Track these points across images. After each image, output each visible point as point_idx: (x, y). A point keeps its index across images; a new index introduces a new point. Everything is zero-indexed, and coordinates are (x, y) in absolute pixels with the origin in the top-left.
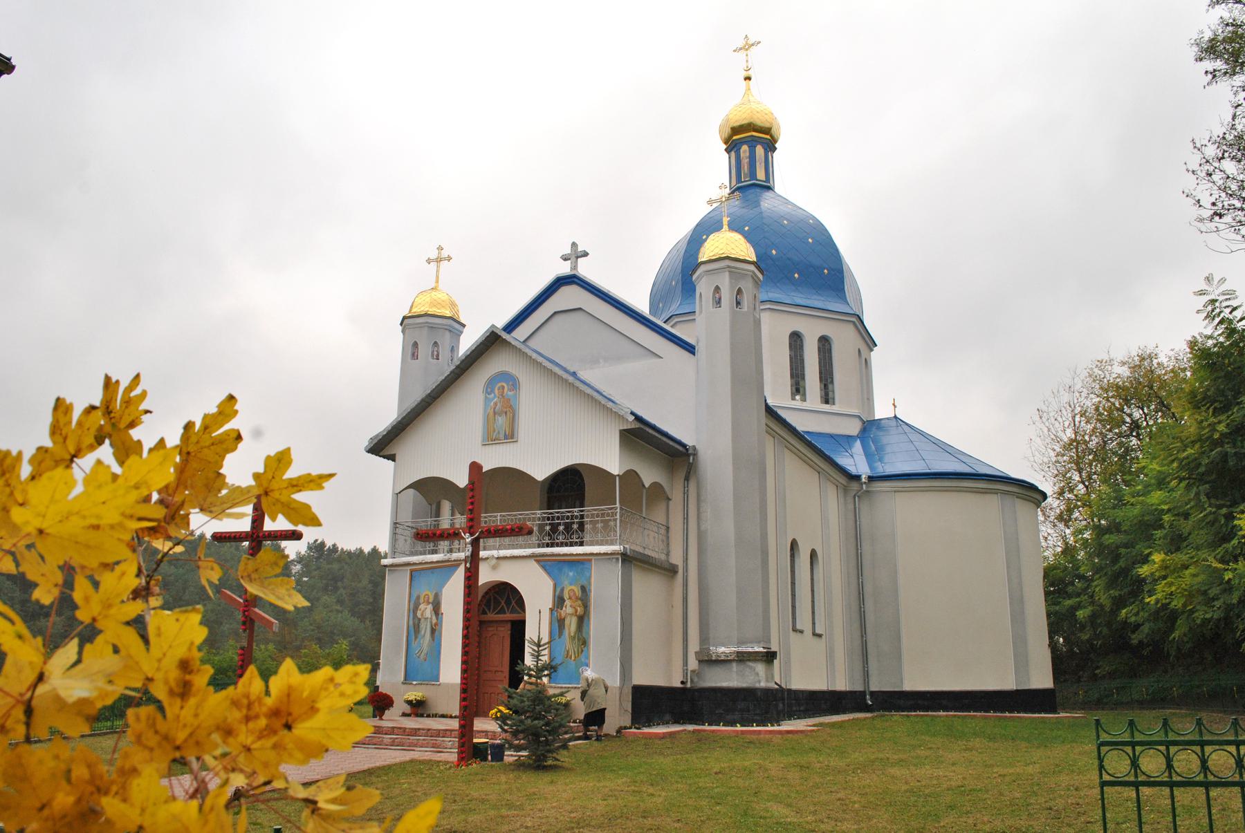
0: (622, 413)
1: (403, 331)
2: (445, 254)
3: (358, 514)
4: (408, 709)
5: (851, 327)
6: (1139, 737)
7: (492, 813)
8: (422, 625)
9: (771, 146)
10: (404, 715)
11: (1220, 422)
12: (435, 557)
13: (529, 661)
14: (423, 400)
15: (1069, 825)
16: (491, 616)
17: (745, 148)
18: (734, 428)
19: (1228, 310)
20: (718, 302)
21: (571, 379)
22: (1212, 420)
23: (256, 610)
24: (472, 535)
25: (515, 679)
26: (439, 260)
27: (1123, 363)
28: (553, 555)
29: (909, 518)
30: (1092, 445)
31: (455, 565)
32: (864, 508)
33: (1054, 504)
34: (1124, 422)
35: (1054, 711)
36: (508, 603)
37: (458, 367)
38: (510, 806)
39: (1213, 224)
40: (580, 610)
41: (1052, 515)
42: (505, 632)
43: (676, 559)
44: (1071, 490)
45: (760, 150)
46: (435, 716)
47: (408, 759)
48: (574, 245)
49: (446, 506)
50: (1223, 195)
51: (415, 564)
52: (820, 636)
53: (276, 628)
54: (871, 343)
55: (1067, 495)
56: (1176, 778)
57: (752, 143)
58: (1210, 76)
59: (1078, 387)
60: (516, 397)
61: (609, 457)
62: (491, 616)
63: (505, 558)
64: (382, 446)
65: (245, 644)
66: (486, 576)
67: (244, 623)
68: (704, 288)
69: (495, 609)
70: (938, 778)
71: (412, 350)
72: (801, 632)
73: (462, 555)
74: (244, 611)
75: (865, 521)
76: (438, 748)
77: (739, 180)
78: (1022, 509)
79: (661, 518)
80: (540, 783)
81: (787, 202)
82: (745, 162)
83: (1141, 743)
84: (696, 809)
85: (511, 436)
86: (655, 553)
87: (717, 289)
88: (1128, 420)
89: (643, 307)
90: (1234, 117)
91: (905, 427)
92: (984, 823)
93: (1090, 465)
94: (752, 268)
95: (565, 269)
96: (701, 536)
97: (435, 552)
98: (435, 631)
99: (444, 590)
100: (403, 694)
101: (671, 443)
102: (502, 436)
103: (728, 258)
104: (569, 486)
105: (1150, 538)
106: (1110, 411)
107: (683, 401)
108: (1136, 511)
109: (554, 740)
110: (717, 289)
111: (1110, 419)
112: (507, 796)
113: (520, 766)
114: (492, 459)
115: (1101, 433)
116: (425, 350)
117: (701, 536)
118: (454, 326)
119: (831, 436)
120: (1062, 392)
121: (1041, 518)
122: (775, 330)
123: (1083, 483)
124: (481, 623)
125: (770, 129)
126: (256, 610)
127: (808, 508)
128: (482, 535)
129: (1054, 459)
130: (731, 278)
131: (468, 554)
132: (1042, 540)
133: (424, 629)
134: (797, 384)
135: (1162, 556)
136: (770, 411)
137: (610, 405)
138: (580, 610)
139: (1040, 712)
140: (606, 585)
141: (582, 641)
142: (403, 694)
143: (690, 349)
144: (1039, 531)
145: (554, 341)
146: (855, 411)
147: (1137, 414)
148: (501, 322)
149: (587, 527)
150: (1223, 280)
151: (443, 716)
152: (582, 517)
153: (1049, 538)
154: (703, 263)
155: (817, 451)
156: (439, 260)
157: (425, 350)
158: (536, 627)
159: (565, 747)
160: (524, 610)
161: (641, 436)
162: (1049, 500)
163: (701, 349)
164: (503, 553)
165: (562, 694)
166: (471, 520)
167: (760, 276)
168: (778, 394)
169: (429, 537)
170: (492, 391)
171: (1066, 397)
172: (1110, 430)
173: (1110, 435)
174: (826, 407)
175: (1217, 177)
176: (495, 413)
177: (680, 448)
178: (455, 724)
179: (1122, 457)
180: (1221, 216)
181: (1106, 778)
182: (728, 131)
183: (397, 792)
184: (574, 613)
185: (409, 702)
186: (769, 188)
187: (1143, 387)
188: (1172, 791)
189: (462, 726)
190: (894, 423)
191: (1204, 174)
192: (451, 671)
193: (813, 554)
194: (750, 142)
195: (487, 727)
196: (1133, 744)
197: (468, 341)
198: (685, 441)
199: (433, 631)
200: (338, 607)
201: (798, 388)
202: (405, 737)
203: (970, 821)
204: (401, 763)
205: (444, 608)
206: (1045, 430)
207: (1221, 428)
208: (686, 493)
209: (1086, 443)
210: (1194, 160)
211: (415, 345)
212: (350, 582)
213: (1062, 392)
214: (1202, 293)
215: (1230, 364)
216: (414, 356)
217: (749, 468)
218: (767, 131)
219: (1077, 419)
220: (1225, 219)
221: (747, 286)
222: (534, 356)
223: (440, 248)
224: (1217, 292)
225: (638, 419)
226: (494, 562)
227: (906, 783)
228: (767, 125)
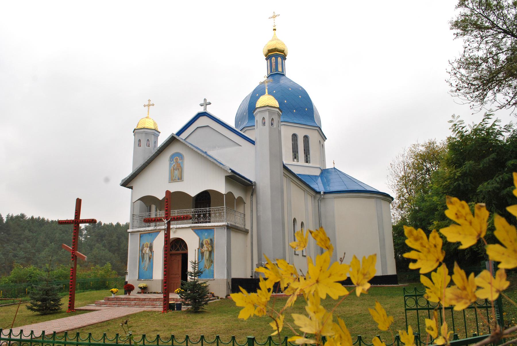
0: (226, 169)
1: (134, 135)
2: (151, 103)
3: (115, 209)
4: (140, 290)
5: (317, 131)
6: (418, 293)
7: (181, 330)
8: (145, 256)
9: (284, 58)
10: (138, 293)
11: (458, 171)
12: (150, 228)
13: (190, 269)
14: (144, 164)
15: (399, 326)
16: (174, 252)
17: (273, 58)
18: (271, 175)
19: (461, 128)
20: (264, 124)
21: (205, 155)
22: (454, 171)
23: (77, 252)
24: (167, 220)
25: (184, 276)
26: (149, 105)
27: (423, 146)
28: (199, 227)
29: (341, 209)
30: (411, 178)
31: (160, 231)
32: (322, 205)
33: (396, 200)
34: (424, 169)
35: (397, 284)
36: (180, 246)
37: (158, 150)
38: (187, 327)
39: (456, 93)
40: (210, 249)
41: (396, 206)
42: (179, 258)
43: (248, 227)
44: (403, 196)
45: (279, 59)
46: (151, 293)
47: (142, 310)
48: (205, 100)
49: (153, 207)
50: (460, 82)
51: (142, 231)
52: (305, 256)
53: (86, 259)
54: (324, 138)
55: (402, 198)
56: (430, 307)
57: (276, 56)
58: (455, 36)
59: (406, 155)
60: (183, 162)
61: (220, 186)
62: (174, 252)
63: (179, 228)
64: (127, 183)
65: (73, 266)
66: (173, 236)
67: (73, 258)
68: (258, 118)
69: (176, 249)
70: (352, 311)
71: (139, 143)
72: (298, 255)
73: (163, 227)
74: (72, 253)
75: (322, 210)
76: (154, 306)
77: (271, 72)
78: (384, 204)
79: (242, 212)
80: (197, 318)
81: (291, 81)
82: (274, 64)
83: (418, 295)
84: (260, 325)
85: (180, 179)
86: (239, 225)
87: (264, 118)
88: (425, 168)
89: (232, 125)
90: (464, 52)
91: (338, 172)
92: (368, 327)
93: (411, 186)
94: (277, 110)
95: (201, 110)
96: (258, 218)
97: (149, 226)
98: (151, 259)
99: (154, 242)
100: (138, 285)
101: (246, 181)
102: (177, 178)
103: (268, 106)
104: (205, 199)
105: (434, 214)
106: (418, 164)
107: (247, 162)
108: (428, 204)
109: (202, 301)
110: (264, 118)
111: (418, 167)
112: (185, 324)
113: (188, 312)
114: (174, 188)
115: (415, 173)
116: (144, 143)
117: (258, 218)
118: (155, 133)
119: (309, 176)
120: (400, 157)
121: (391, 207)
122: (286, 132)
123: (408, 193)
124: (171, 255)
125: (284, 51)
126: (77, 252)
127: (300, 204)
128: (170, 219)
129: (397, 184)
130: (269, 114)
131: (166, 227)
132: (392, 215)
133: (147, 257)
134: (295, 155)
135: (437, 222)
136: (285, 167)
137: (221, 166)
138: (210, 249)
139: (391, 284)
140: (220, 238)
141: (211, 261)
142: (138, 285)
143: (253, 142)
144: (390, 212)
145: (195, 139)
146: (318, 166)
147: (428, 166)
148: (175, 131)
149: (213, 215)
150: (459, 116)
151: (155, 293)
152: (210, 211)
153: (395, 215)
154: (258, 108)
155: (302, 181)
156: (149, 105)
157: (144, 143)
158: (192, 256)
159: (206, 304)
160: (187, 249)
161: (234, 178)
162: (395, 200)
163: (257, 143)
164: (178, 226)
165: (205, 283)
166: (166, 214)
167: (281, 113)
168: (288, 160)
169: (148, 221)
170: (173, 160)
171: (401, 159)
172: (418, 172)
173: (418, 174)
174: (307, 164)
175: (458, 75)
176: (174, 169)
177: (249, 183)
178: (161, 296)
179: (423, 183)
180: (459, 90)
181: (407, 308)
182: (266, 51)
183: (140, 324)
184: (208, 249)
185: (141, 288)
186: (283, 75)
187: (430, 155)
188: (429, 312)
189: (164, 297)
190: (334, 170)
191: (453, 74)
192: (158, 274)
193: (302, 224)
194: (276, 56)
195: (175, 297)
196: (416, 296)
197: (161, 140)
198: (251, 180)
199: (150, 259)
200: (103, 248)
201: (295, 156)
202: (140, 302)
203: (364, 326)
204: (140, 313)
205: (154, 249)
206: (393, 172)
207: (458, 174)
208: (252, 201)
209: (409, 177)
210: (450, 68)
211: (140, 141)
212: (113, 239)
213: (400, 157)
214: (451, 121)
215: (461, 149)
216: (139, 145)
217: (278, 191)
218: (283, 51)
219: (406, 167)
220: (461, 91)
221: (276, 118)
222: (190, 146)
223: (149, 101)
224: (457, 121)
225: (233, 171)
226: (175, 230)
227: (340, 313)
228: (283, 49)
